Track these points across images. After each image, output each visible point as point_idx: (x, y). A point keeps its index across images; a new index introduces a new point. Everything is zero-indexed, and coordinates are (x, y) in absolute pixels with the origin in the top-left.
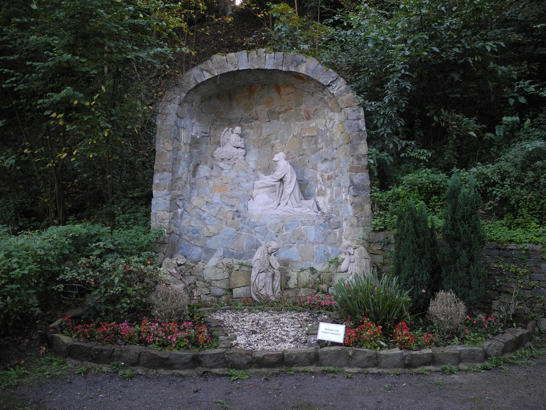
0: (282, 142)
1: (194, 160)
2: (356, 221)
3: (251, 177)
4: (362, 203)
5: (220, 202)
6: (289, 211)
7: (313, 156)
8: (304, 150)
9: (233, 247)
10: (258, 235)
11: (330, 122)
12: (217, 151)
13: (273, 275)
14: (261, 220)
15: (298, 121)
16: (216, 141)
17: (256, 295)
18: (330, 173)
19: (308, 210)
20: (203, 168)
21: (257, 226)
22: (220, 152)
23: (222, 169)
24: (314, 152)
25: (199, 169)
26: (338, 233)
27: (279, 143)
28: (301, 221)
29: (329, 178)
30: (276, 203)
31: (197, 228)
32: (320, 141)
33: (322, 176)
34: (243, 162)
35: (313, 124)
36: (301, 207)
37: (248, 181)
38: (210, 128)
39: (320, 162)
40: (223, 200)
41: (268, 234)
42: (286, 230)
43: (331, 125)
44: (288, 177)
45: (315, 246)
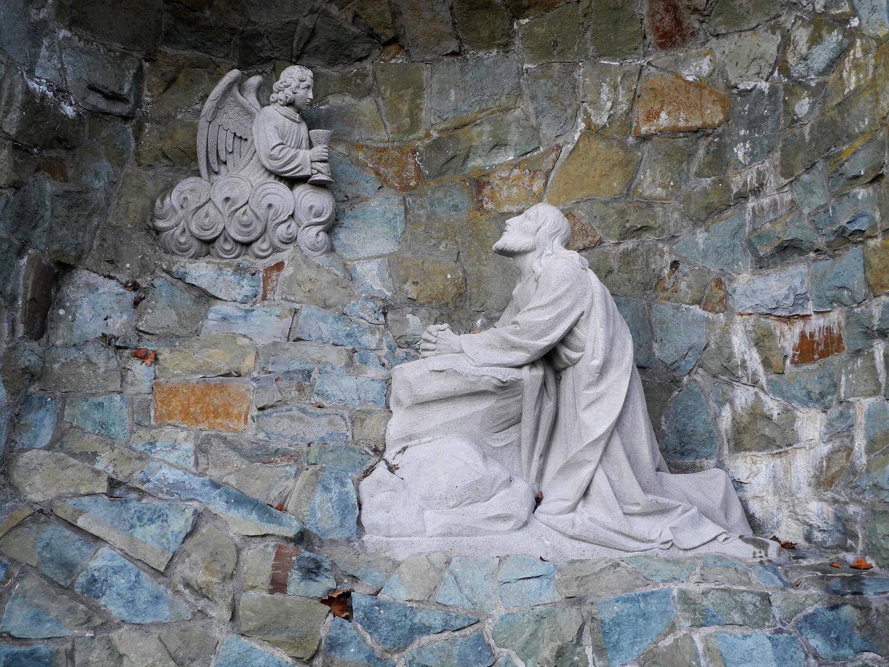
0: (527, 162)
1: (39, 237)
3: (369, 340)
5: (196, 483)
6: (604, 534)
7: (701, 236)
8: (649, 203)
11: (815, 40)
12: (173, 200)
14: (449, 595)
15: (612, 55)
16: (167, 145)
18: (816, 324)
19: (710, 529)
20: (92, 288)
21: (426, 630)
22: (188, 204)
23: (205, 297)
24: (709, 213)
25: (69, 291)
27: (515, 165)
28: (685, 598)
29: (807, 350)
30: (522, 488)
31: (43, 649)
32: (740, 152)
33: (762, 341)
34: (321, 259)
35: (697, 67)
36: (664, 511)
37: (355, 359)
38: (139, 77)
39: (746, 262)
40: (214, 473)
43: (821, 56)
44: (593, 338)
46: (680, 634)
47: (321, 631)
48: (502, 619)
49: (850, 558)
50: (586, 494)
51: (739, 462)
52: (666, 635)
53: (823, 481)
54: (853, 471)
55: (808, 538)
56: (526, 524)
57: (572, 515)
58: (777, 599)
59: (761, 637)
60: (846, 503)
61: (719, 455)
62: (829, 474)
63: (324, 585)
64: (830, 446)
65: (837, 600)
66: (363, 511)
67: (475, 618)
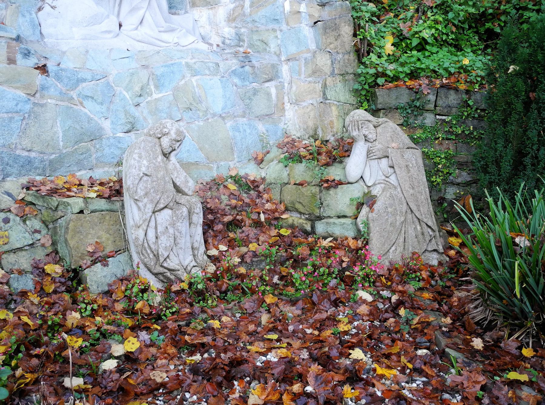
2: (329, 62)
4: (337, 21)
9: (26, 143)
10: (88, 104)
13: (190, 213)
14: (91, 65)
17: (156, 275)
21: (84, 80)
26: (273, 91)
28: (188, 65)
36: (172, 30)
41: (117, 100)
42: (157, 87)
45: (229, 124)
46: (187, 79)
47: (37, 82)
48: (116, 75)
49: (241, 49)
50: (141, 23)
51: (195, 12)
52: (182, 80)
53: (231, 19)
54: (244, 15)
55: (223, 43)
56: (118, 35)
57: (136, 32)
58: (221, 65)
59: (217, 79)
60: (241, 28)
61: (186, 9)
62: (234, 16)
63: (33, 61)
64: (234, 5)
65: (243, 64)
66: (42, 27)
67: (105, 75)
